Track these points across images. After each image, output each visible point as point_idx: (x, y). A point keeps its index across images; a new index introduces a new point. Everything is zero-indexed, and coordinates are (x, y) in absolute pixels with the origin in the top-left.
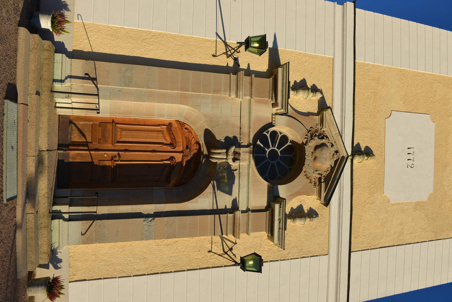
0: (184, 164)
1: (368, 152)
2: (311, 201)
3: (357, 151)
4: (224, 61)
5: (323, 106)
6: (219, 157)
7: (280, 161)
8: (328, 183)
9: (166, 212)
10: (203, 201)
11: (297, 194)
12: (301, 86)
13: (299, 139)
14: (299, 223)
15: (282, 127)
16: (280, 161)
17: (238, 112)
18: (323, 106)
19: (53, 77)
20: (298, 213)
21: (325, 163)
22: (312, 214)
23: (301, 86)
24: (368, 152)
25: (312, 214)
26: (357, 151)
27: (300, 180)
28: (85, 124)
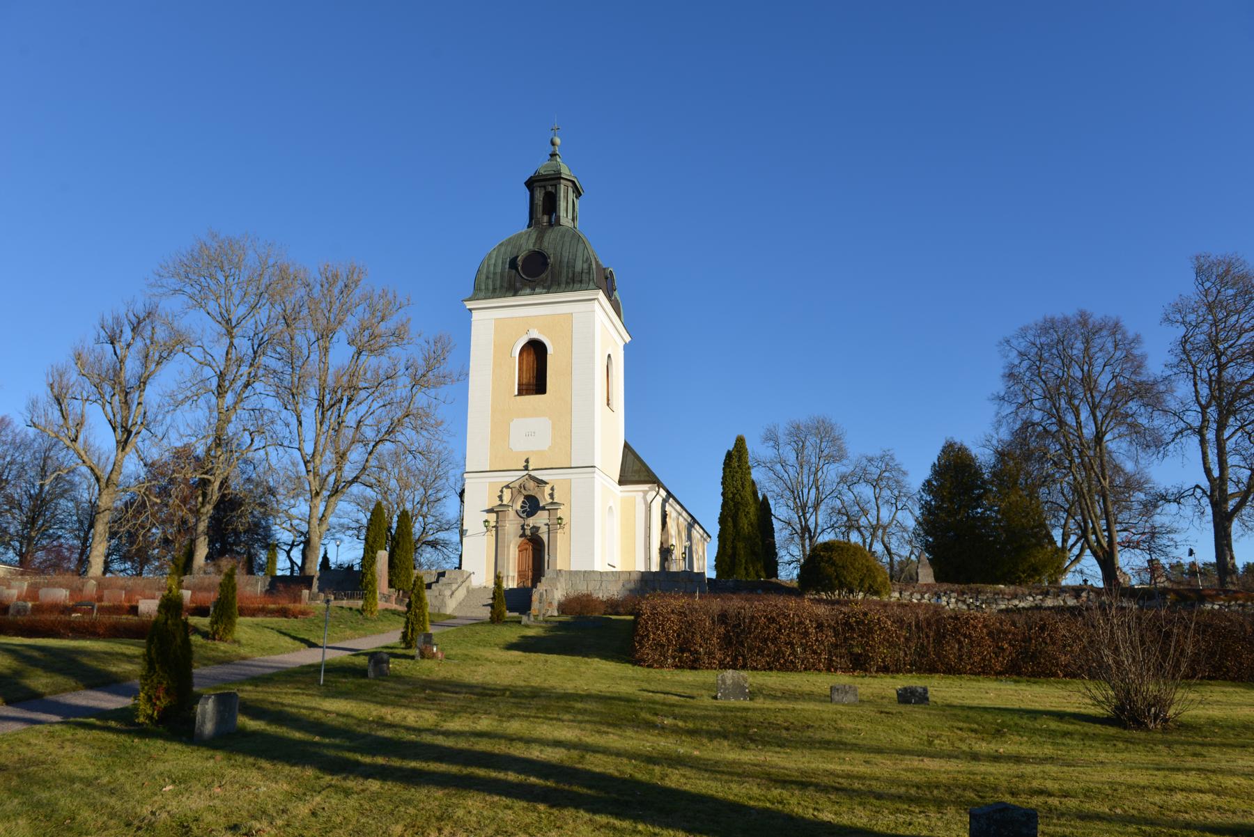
0: (395, 525)
1: (527, 461)
2: (547, 489)
3: (526, 468)
4: (494, 532)
5: (507, 487)
6: (528, 532)
7: (532, 506)
8: (541, 483)
9: (302, 667)
10: (545, 537)
11: (545, 500)
12: (500, 498)
13: (522, 499)
14: (556, 496)
15: (518, 506)
16: (532, 506)
17: (512, 525)
18: (507, 487)
19: (482, 623)
20: (552, 496)
21: (532, 484)
22: (552, 489)
23: (500, 498)
24: (527, 461)
25: (552, 489)
26: (526, 468)
27: (539, 496)
28: (394, 704)
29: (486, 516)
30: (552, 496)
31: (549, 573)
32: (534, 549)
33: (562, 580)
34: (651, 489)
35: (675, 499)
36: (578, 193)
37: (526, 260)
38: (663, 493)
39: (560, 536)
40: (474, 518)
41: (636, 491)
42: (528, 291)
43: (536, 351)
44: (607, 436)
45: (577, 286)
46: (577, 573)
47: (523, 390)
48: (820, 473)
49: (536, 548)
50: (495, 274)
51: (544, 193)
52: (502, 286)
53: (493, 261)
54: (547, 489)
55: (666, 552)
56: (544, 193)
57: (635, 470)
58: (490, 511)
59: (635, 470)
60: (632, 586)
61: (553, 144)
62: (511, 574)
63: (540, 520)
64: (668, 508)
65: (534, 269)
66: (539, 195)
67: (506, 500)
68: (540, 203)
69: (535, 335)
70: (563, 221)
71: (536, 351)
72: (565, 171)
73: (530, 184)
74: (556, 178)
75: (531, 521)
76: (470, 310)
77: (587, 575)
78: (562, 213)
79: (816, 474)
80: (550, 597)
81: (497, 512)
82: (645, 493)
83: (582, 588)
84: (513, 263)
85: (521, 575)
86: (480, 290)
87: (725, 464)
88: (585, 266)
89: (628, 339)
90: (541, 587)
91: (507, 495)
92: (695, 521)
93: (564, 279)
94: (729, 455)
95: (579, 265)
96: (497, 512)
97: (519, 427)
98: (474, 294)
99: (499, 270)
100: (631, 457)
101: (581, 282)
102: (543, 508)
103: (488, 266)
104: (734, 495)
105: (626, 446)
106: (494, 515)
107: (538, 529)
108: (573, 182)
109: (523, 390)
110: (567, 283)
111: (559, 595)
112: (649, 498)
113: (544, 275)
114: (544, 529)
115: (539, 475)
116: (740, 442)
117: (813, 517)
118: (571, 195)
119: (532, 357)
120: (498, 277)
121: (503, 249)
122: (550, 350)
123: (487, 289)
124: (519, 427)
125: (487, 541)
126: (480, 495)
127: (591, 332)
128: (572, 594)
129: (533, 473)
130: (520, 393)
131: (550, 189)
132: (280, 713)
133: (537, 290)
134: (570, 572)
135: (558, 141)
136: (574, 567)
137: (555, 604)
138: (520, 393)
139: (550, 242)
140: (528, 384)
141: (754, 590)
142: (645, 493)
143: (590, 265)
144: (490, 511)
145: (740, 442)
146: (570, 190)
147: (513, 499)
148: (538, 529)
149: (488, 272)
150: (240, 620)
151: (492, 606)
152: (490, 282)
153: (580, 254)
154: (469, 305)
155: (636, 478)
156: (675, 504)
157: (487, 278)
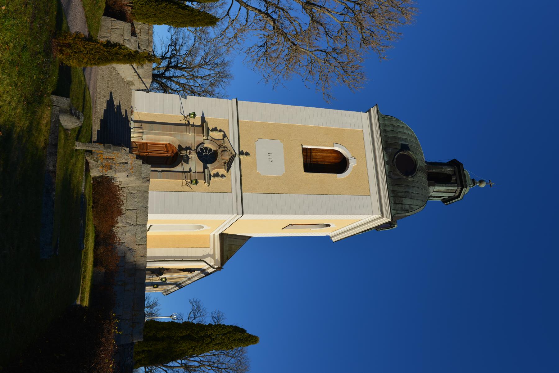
1: (247, 154)
2: (222, 171)
3: (241, 153)
4: (184, 122)
5: (225, 136)
6: (183, 153)
7: (208, 157)
8: (228, 166)
11: (213, 169)
12: (215, 129)
14: (217, 179)
15: (208, 145)
16: (208, 157)
17: (190, 138)
18: (225, 136)
20: (217, 175)
21: (227, 157)
22: (223, 176)
23: (215, 129)
24: (247, 154)
25: (223, 176)
26: (241, 153)
27: (216, 163)
29: (199, 116)
30: (217, 175)
31: (148, 168)
32: (167, 158)
33: (139, 183)
34: (216, 261)
35: (203, 277)
36: (445, 201)
37: (409, 158)
38: (211, 270)
39: (179, 182)
40: (196, 104)
41: (214, 249)
43: (339, 164)
44: (262, 224)
46: (146, 199)
47: (306, 152)
48: (209, 368)
49: (167, 160)
50: (397, 132)
51: (450, 173)
52: (388, 137)
53: (406, 131)
54: (222, 171)
55: (159, 272)
56: (450, 173)
57: (230, 244)
58: (203, 119)
59: (230, 244)
60: (130, 258)
61: (481, 182)
62: (145, 136)
63: (195, 164)
64: (196, 272)
65: (400, 164)
66: (448, 170)
67: (214, 135)
68: (443, 171)
69: (352, 164)
70: (431, 189)
71: (339, 164)
72: (466, 191)
73: (455, 163)
74: (462, 184)
75: (193, 156)
76: (369, 111)
77: (144, 210)
78: (437, 188)
79: (209, 366)
80: (118, 167)
81: (202, 126)
82: (213, 256)
83: (128, 205)
84: (405, 147)
85: (144, 146)
86: (384, 120)
87: (236, 327)
88: (407, 207)
89: (334, 239)
90: (130, 158)
91: (217, 135)
92: (180, 288)
93: (396, 188)
94: (243, 331)
95: (407, 201)
96: (202, 126)
97: (276, 147)
98: (381, 116)
99: (400, 136)
101: (395, 203)
102: (205, 167)
103: (402, 127)
104: (210, 336)
106: (199, 124)
107: (187, 162)
108: (458, 197)
109: (306, 152)
111: (121, 178)
112: (208, 260)
113: (398, 172)
114: (186, 167)
115: (235, 164)
117: (177, 364)
118: (446, 195)
119: (333, 160)
121: (413, 140)
122: (340, 176)
123: (386, 125)
125: (176, 116)
126: (216, 110)
127: (353, 209)
128: (123, 194)
129: (237, 159)
130: (304, 150)
131: (454, 178)
132: (62, 20)
133: (387, 166)
134: (146, 192)
135: (483, 185)
136: (152, 195)
137: (110, 174)
138: (304, 150)
139: (421, 177)
140: (311, 157)
142: (213, 256)
143: (409, 212)
144: (203, 119)
145: (253, 339)
146: (452, 195)
147: (213, 140)
148: (187, 162)
149: (398, 127)
150: (146, 288)
151: (90, 39)
152: (390, 128)
153: (415, 202)
154: (373, 110)
155: (226, 248)
156: (199, 277)
157: (394, 126)
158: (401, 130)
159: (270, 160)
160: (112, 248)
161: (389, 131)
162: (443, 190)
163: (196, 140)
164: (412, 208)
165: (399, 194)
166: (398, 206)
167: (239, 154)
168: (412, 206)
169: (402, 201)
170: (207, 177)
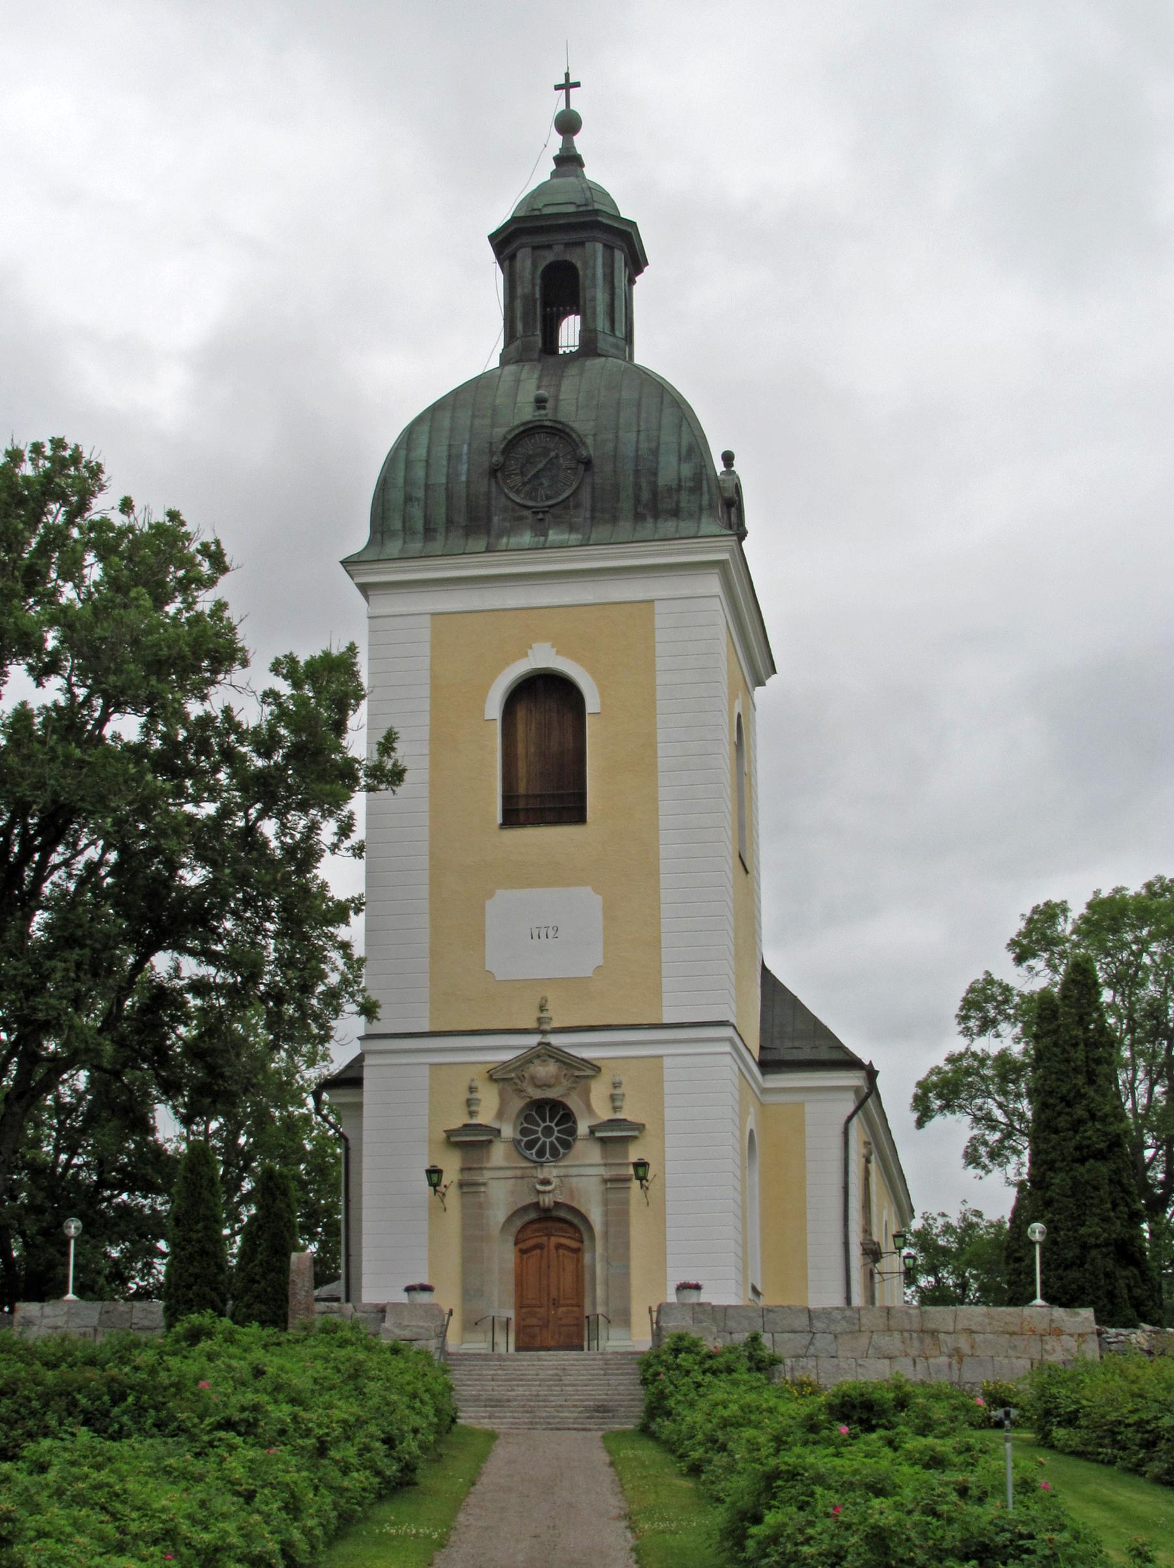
7: (549, 1121)
27: (574, 1103)
42: (527, 538)
43: (547, 700)
45: (668, 526)
52: (450, 522)
54: (599, 1092)
69: (543, 657)
71: (547, 700)
97: (509, 913)
100: (824, 1054)
103: (409, 464)
105: (742, 535)
110: (639, 517)
116: (920, 1124)
120: (441, 495)
124: (509, 913)
129: (555, 1040)
130: (513, 816)
138: (513, 816)
141: (136, 751)
152: (417, 512)
157: (408, 499)
158: (419, 473)
159: (543, 935)
160: (1043, 1010)
161: (427, 520)
162: (607, 297)
163: (502, 1163)
164: (690, 450)
165: (645, 496)
166: (683, 504)
167: (544, 1032)
168: (684, 451)
169: (669, 489)
170: (616, 1136)
